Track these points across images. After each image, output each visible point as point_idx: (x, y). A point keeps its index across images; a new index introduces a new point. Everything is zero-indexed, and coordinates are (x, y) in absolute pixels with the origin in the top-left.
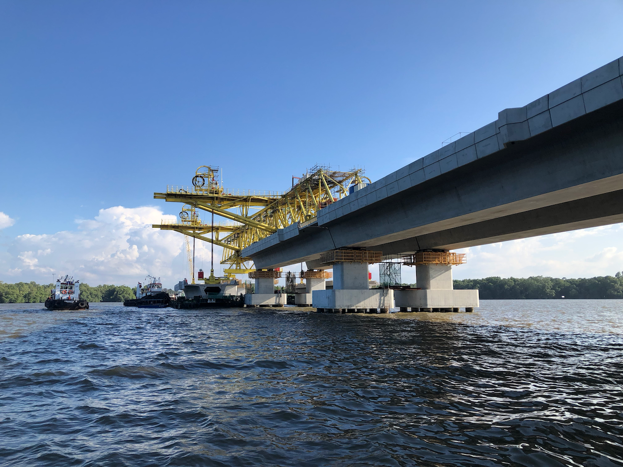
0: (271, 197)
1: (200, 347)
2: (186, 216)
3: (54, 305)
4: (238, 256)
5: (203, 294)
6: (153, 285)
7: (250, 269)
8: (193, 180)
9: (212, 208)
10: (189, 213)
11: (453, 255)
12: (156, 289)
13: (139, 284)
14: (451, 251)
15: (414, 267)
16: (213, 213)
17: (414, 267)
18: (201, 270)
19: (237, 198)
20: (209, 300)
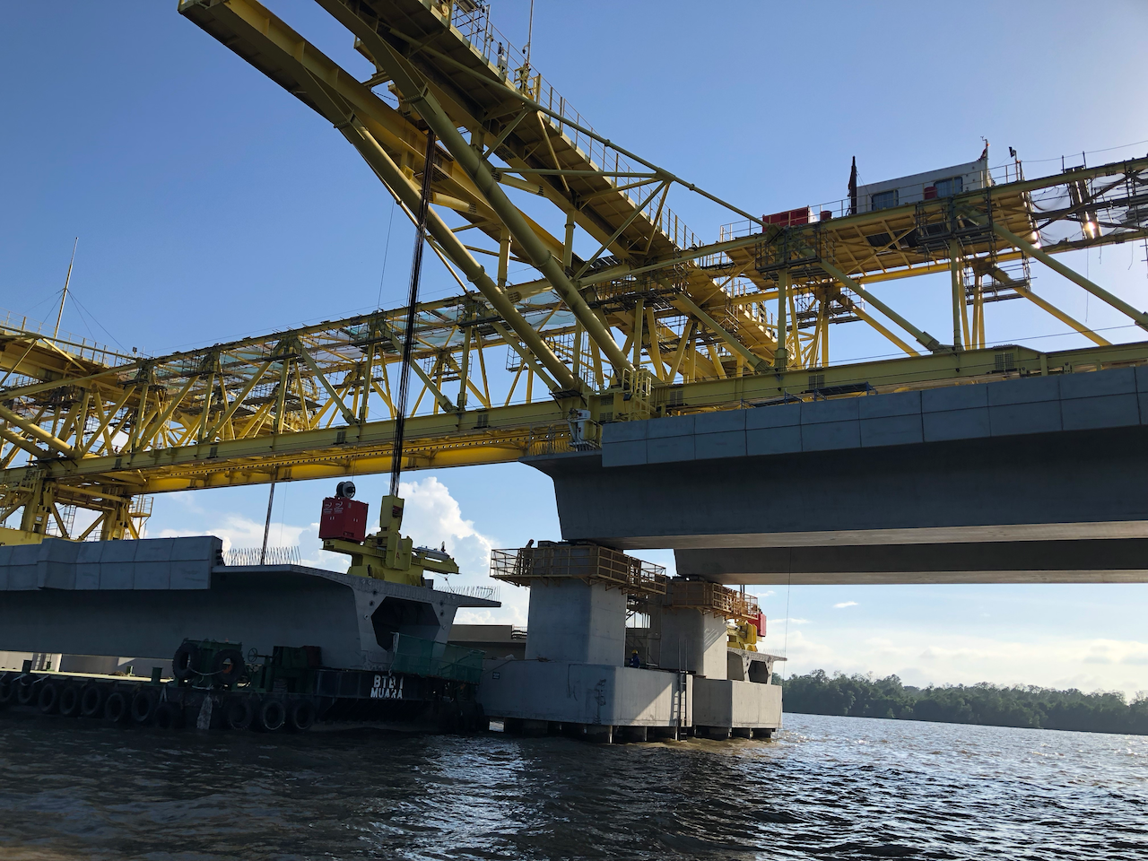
20: (377, 681)
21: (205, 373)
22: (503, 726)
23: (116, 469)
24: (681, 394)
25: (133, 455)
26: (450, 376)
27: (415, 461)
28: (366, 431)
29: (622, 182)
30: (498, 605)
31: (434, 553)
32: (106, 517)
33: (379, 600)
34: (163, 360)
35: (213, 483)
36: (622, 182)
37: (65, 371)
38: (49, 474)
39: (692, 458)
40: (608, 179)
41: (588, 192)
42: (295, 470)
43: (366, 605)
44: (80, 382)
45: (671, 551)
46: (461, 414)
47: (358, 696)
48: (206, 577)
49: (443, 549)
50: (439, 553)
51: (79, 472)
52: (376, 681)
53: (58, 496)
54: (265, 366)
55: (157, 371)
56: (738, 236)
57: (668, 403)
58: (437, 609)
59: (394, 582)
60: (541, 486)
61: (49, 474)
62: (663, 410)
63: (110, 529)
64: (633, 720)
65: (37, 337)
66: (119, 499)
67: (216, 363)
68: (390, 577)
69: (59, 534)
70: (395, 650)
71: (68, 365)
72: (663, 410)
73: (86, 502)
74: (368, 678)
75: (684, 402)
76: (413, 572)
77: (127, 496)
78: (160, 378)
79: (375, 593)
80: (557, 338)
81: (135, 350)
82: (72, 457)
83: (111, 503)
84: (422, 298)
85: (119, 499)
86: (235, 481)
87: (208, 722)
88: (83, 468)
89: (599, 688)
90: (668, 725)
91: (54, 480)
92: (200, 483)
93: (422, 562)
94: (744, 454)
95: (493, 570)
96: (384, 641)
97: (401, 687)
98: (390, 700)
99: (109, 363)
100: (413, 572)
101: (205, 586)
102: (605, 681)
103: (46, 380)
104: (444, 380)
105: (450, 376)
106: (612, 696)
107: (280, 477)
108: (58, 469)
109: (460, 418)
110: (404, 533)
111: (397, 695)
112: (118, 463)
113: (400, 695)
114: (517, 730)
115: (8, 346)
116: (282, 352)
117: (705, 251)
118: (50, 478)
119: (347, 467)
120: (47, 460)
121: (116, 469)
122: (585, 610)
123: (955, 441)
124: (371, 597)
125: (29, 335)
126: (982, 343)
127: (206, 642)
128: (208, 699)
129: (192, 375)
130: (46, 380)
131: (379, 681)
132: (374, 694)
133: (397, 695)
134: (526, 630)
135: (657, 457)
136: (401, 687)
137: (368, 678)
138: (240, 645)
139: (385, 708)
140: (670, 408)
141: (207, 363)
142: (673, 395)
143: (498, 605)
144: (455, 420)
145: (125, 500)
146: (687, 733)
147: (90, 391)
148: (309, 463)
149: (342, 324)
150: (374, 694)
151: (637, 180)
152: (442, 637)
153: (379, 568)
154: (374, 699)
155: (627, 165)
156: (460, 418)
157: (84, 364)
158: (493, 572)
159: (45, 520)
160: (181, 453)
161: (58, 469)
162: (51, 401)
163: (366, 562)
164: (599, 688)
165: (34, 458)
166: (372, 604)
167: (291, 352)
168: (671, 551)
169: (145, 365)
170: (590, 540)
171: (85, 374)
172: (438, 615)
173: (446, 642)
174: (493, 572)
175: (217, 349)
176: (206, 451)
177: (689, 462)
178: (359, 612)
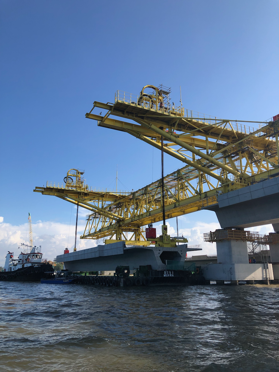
0: (121, 194)
1: (52, 293)
2: (70, 181)
3: (223, 240)
4: (120, 226)
5: (158, 264)
6: (33, 254)
7: (130, 240)
8: (64, 178)
9: (78, 200)
10: (73, 178)
11: (248, 233)
12: (35, 260)
13: (10, 253)
14: (245, 229)
15: (215, 243)
16: (78, 205)
17: (215, 243)
18: (67, 249)
19: (96, 194)
20: (165, 272)
21: (145, 194)
22: (211, 283)
23: (132, 221)
24: (254, 178)
25: (134, 217)
26: (204, 182)
27: (199, 208)
28: (180, 203)
29: (217, 125)
30: (201, 249)
31: (180, 238)
32: (135, 233)
33: (161, 252)
34: (137, 192)
35: (156, 221)
36: (217, 125)
37: (118, 199)
38: (120, 225)
39: (239, 202)
40: (213, 126)
41: (209, 130)
42: (173, 214)
43: (157, 254)
44: (121, 201)
45: (271, 225)
46: (201, 194)
47: (160, 276)
48: (122, 251)
49: (183, 236)
50: (181, 238)
51: (125, 223)
52: (165, 272)
53: (123, 230)
54: (157, 189)
55: (137, 195)
56: (262, 127)
57: (251, 182)
58: (180, 253)
59: (167, 247)
60: (213, 214)
61: (120, 225)
62: (250, 184)
63: (136, 236)
64: (244, 279)
65: (109, 193)
66: (137, 228)
67: (147, 191)
68: (165, 246)
69: (125, 239)
70: (167, 264)
71: (118, 197)
72: (250, 184)
73: (130, 230)
74: (162, 272)
75: (256, 180)
76: (173, 243)
77: (139, 227)
78: (137, 196)
79: (160, 250)
80: (117, 210)
81: (133, 190)
82: (123, 220)
83: (135, 230)
84: (165, 175)
85: (137, 228)
86: (160, 220)
87: (123, 285)
88: (126, 222)
89: (231, 270)
90: (261, 279)
91: (121, 226)
92: (153, 221)
93: (175, 241)
94: (251, 199)
95: (204, 239)
96: (164, 262)
97: (173, 273)
98: (170, 277)
99: (127, 195)
100: (173, 243)
101: (122, 253)
102: (231, 268)
103: (116, 201)
104: (203, 183)
105: (204, 182)
106: (234, 272)
107: (170, 217)
108: (121, 223)
109: (200, 196)
110: (168, 234)
111: (172, 276)
112: (132, 220)
113: (173, 275)
114: (220, 283)
115: (104, 196)
116: (160, 185)
117: (255, 133)
118: (120, 226)
119: (184, 212)
120: (119, 221)
121: (132, 221)
122: (230, 248)
123: (235, 204)
124: (159, 252)
125: (107, 193)
126: (188, 197)
127: (120, 266)
128: (122, 279)
129: (143, 194)
130: (116, 201)
131: (166, 272)
132: (164, 276)
133: (172, 276)
134: (217, 255)
135: (232, 203)
136: (173, 273)
137: (162, 272)
138: (129, 266)
139: (168, 279)
140: (252, 183)
141: (145, 190)
142: (252, 179)
143: (201, 249)
144: (199, 196)
145: (138, 228)
146: (272, 282)
147: (124, 202)
148: (191, 208)
149: (172, 174)
150: (164, 276)
151: (219, 124)
152: (182, 260)
153: (162, 244)
154: (165, 277)
155: (217, 122)
156: (200, 196)
157: (121, 196)
158: (205, 240)
159: (121, 236)
160: (144, 215)
161: (121, 223)
162: (119, 206)
163: (158, 243)
164: (231, 270)
165: (116, 221)
166: (159, 253)
167: (179, 176)
168: (271, 225)
169: (133, 194)
170: (228, 228)
171: (122, 198)
172: (181, 254)
173: (184, 261)
174: (205, 240)
175: (147, 186)
176: (148, 214)
177: (239, 203)
178: (156, 256)
